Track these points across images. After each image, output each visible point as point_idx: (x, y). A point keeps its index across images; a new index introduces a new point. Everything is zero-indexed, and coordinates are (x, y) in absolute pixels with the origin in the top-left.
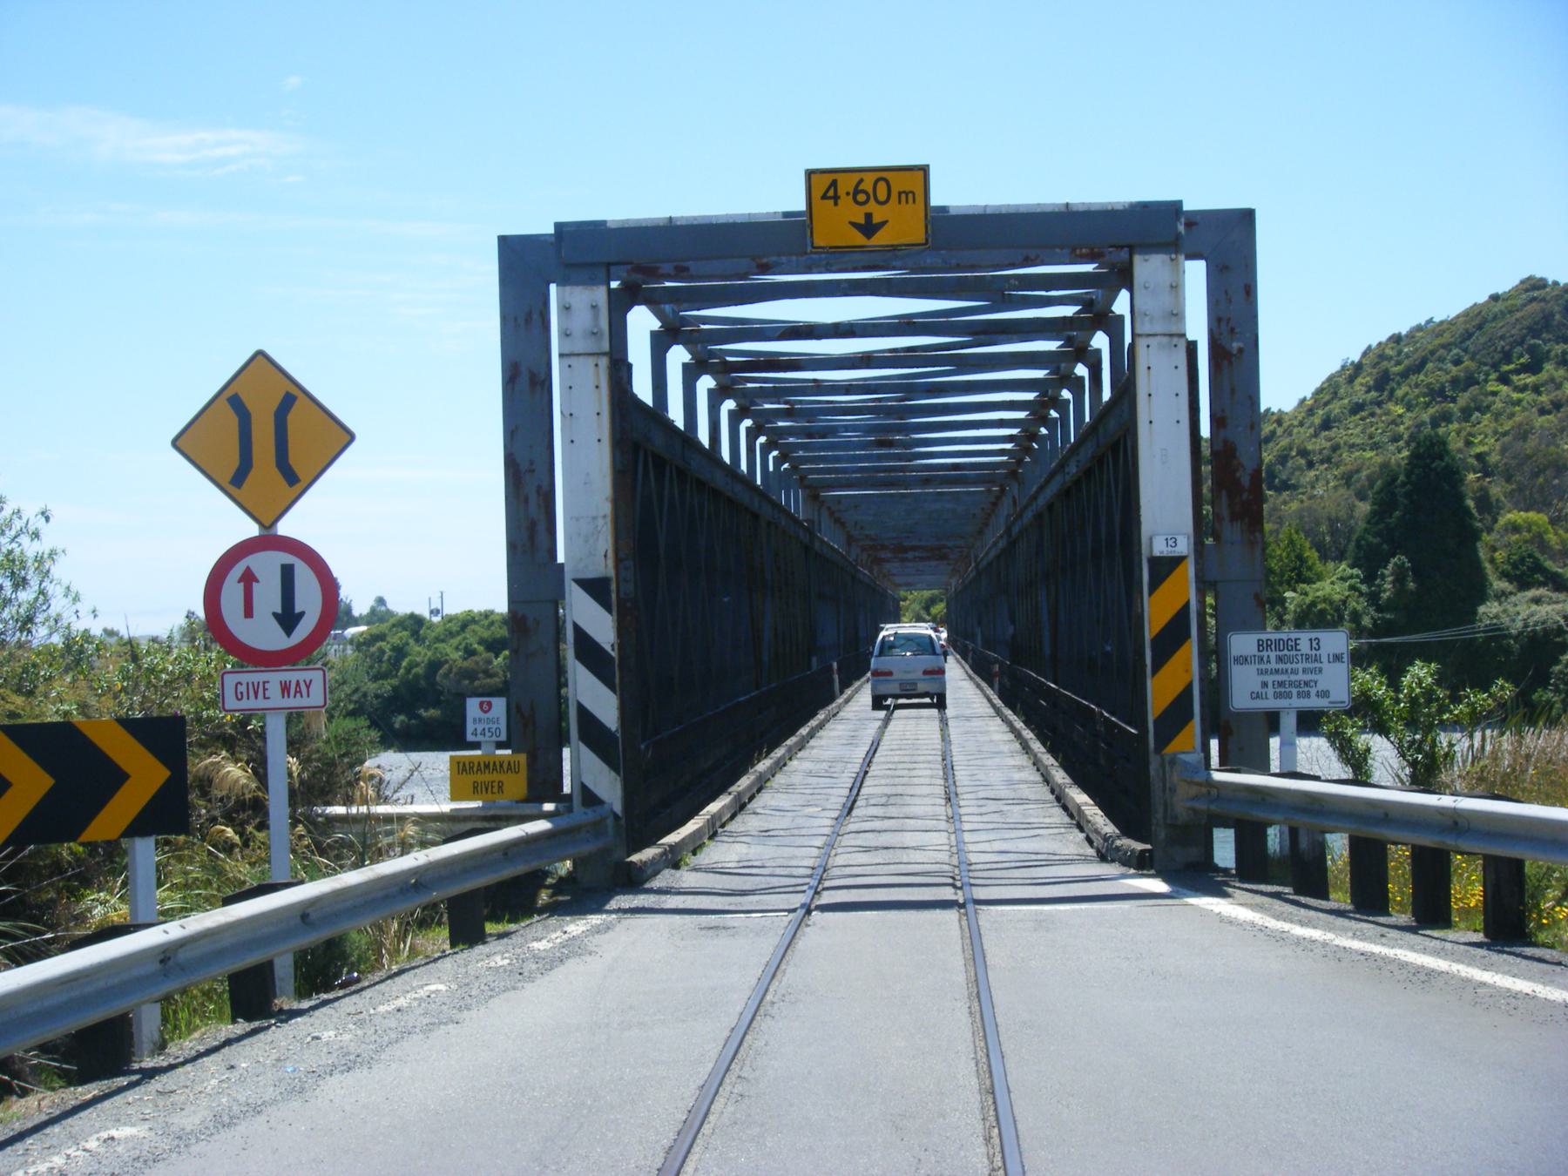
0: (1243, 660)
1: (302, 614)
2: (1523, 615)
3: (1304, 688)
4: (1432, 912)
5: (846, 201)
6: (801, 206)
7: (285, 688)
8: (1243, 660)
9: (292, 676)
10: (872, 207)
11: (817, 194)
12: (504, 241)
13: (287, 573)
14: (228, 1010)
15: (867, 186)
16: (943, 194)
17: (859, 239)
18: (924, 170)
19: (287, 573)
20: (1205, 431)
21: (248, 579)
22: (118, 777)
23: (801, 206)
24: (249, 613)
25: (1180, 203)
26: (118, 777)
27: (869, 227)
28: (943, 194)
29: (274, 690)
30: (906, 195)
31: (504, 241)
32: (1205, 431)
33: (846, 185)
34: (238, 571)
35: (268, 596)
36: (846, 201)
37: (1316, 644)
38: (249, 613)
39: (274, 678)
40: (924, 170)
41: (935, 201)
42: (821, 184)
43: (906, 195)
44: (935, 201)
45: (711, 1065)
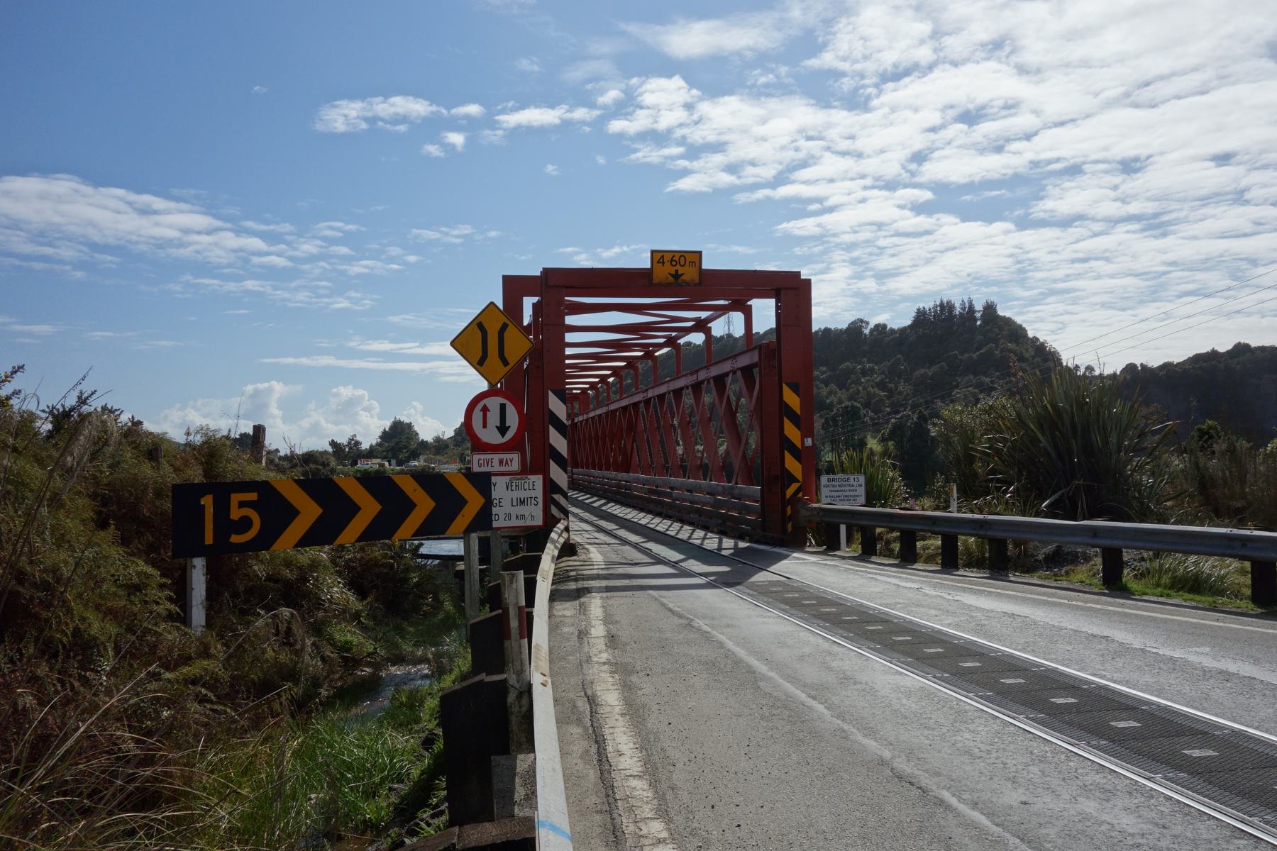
1: (333, 443)
4: (908, 557)
6: (649, 266)
7: (501, 462)
9: (504, 456)
10: (678, 267)
11: (656, 260)
12: (505, 278)
13: (503, 407)
14: (1098, 580)
15: (676, 258)
18: (700, 253)
21: (485, 410)
22: (354, 509)
23: (649, 266)
24: (485, 426)
25: (798, 273)
26: (354, 509)
27: (676, 276)
28: (706, 265)
29: (496, 463)
31: (505, 278)
34: (480, 406)
35: (494, 419)
38: (485, 426)
39: (496, 457)
40: (700, 253)
41: (704, 266)
44: (704, 266)
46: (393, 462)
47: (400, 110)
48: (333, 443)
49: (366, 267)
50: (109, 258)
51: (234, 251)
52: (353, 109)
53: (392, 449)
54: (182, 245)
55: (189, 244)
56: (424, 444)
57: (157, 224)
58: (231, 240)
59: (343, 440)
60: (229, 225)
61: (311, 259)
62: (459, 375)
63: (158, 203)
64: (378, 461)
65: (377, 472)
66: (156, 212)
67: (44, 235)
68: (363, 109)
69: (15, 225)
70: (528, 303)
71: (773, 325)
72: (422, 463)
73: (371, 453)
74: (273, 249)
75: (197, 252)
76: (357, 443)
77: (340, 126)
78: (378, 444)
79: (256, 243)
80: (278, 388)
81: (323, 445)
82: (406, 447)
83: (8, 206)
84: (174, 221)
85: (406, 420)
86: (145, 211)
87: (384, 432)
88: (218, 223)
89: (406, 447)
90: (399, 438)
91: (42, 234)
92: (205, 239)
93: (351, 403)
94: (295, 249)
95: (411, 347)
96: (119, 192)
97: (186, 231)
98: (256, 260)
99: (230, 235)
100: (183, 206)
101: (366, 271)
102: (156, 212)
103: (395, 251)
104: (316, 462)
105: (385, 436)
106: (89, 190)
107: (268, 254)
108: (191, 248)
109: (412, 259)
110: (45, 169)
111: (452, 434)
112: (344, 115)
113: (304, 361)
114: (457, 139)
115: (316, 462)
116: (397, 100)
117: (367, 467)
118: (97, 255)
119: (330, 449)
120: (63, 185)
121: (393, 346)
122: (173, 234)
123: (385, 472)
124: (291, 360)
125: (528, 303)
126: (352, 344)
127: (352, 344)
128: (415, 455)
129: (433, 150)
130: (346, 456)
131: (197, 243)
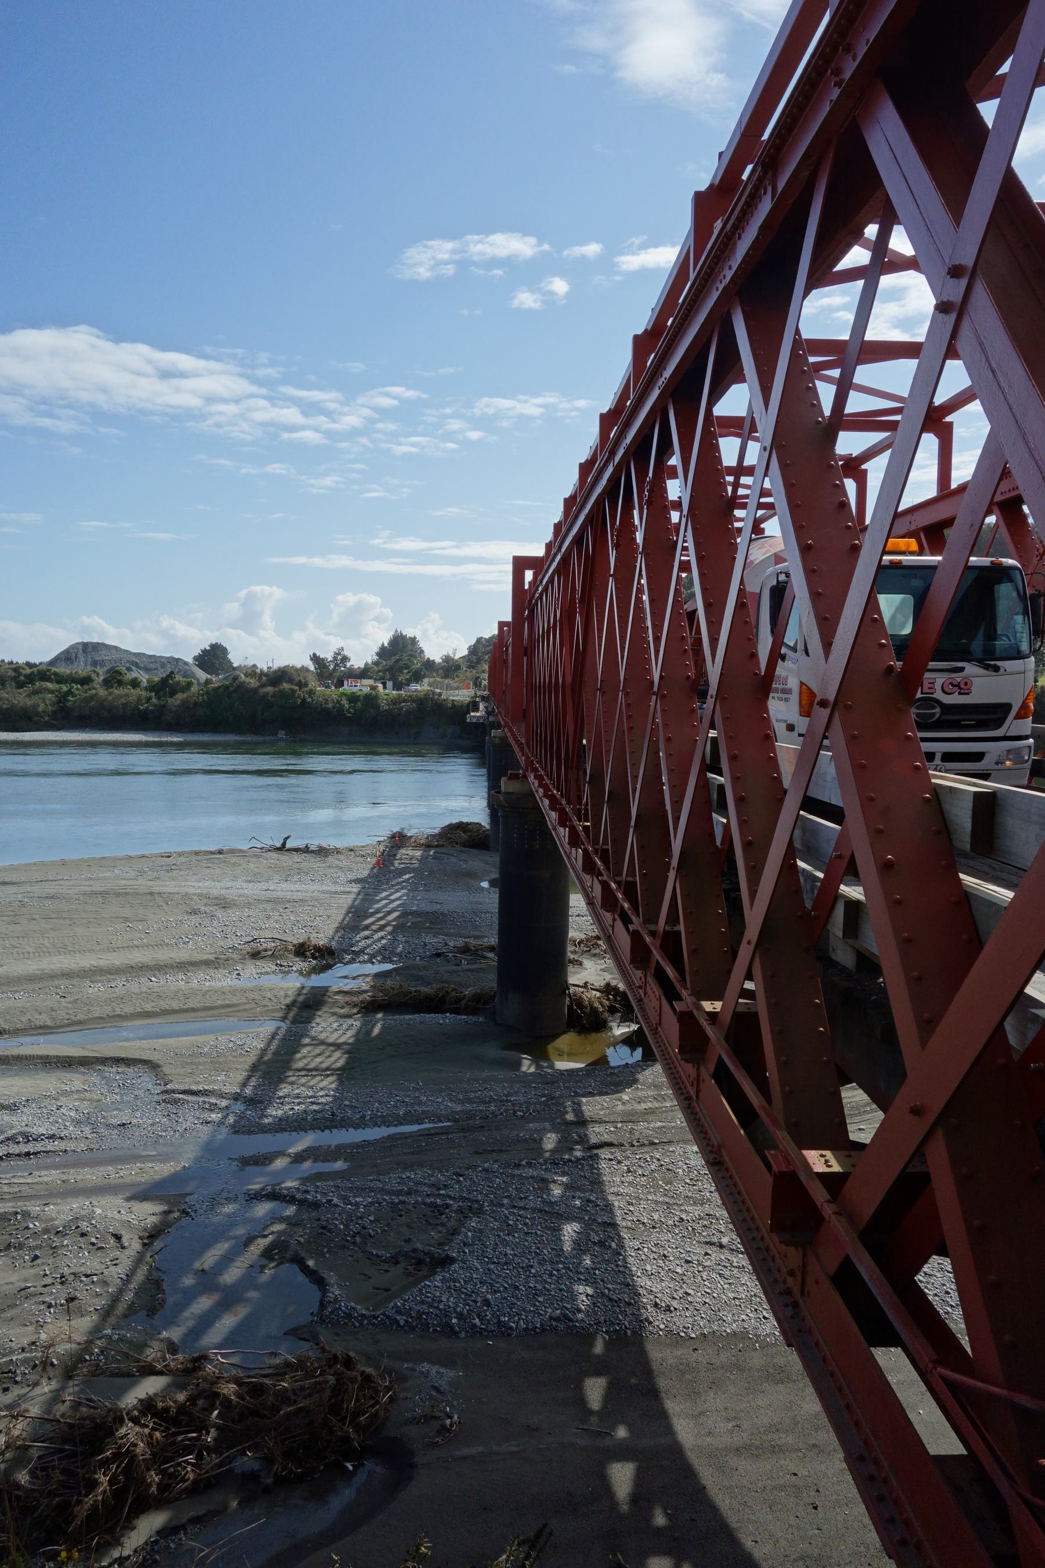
1: (315, 658)
46: (390, 684)
47: (502, 253)
48: (315, 658)
49: (413, 445)
50: (115, 431)
51: (263, 424)
52: (444, 249)
53: (390, 669)
54: (202, 416)
55: (211, 414)
56: (429, 664)
57: (178, 390)
58: (265, 412)
59: (328, 655)
60: (264, 391)
61: (353, 433)
62: (495, 582)
63: (183, 361)
64: (370, 682)
65: (367, 697)
66: (183, 375)
67: (47, 404)
68: (454, 252)
69: (15, 390)
70: (529, 575)
71: (496, 632)
72: (426, 687)
73: (364, 673)
74: (310, 421)
75: (218, 425)
76: (345, 659)
77: (424, 272)
78: (376, 663)
79: (291, 415)
80: (277, 593)
81: (301, 659)
82: (407, 667)
83: (18, 370)
84: (204, 384)
85: (409, 633)
86: (166, 374)
87: (383, 648)
88: (253, 389)
89: (407, 667)
90: (366, 664)
91: (44, 401)
92: (231, 409)
93: (359, 608)
94: (334, 421)
95: (446, 547)
96: (144, 349)
97: (211, 399)
98: (286, 436)
99: (263, 403)
100: (213, 365)
101: (413, 450)
102: (183, 375)
103: (455, 425)
104: (291, 681)
105: (383, 653)
106: (108, 346)
107: (303, 428)
108: (209, 422)
109: (474, 435)
110: (63, 321)
111: (465, 652)
112: (427, 258)
113: (317, 561)
114: (560, 286)
115: (291, 681)
116: (498, 238)
117: (355, 689)
118: (102, 429)
119: (312, 667)
120: (79, 339)
121: (425, 545)
122: (194, 402)
123: (377, 697)
124: (301, 560)
125: (529, 575)
126: (377, 541)
127: (377, 541)
128: (417, 677)
129: (526, 299)
130: (330, 676)
131: (221, 413)
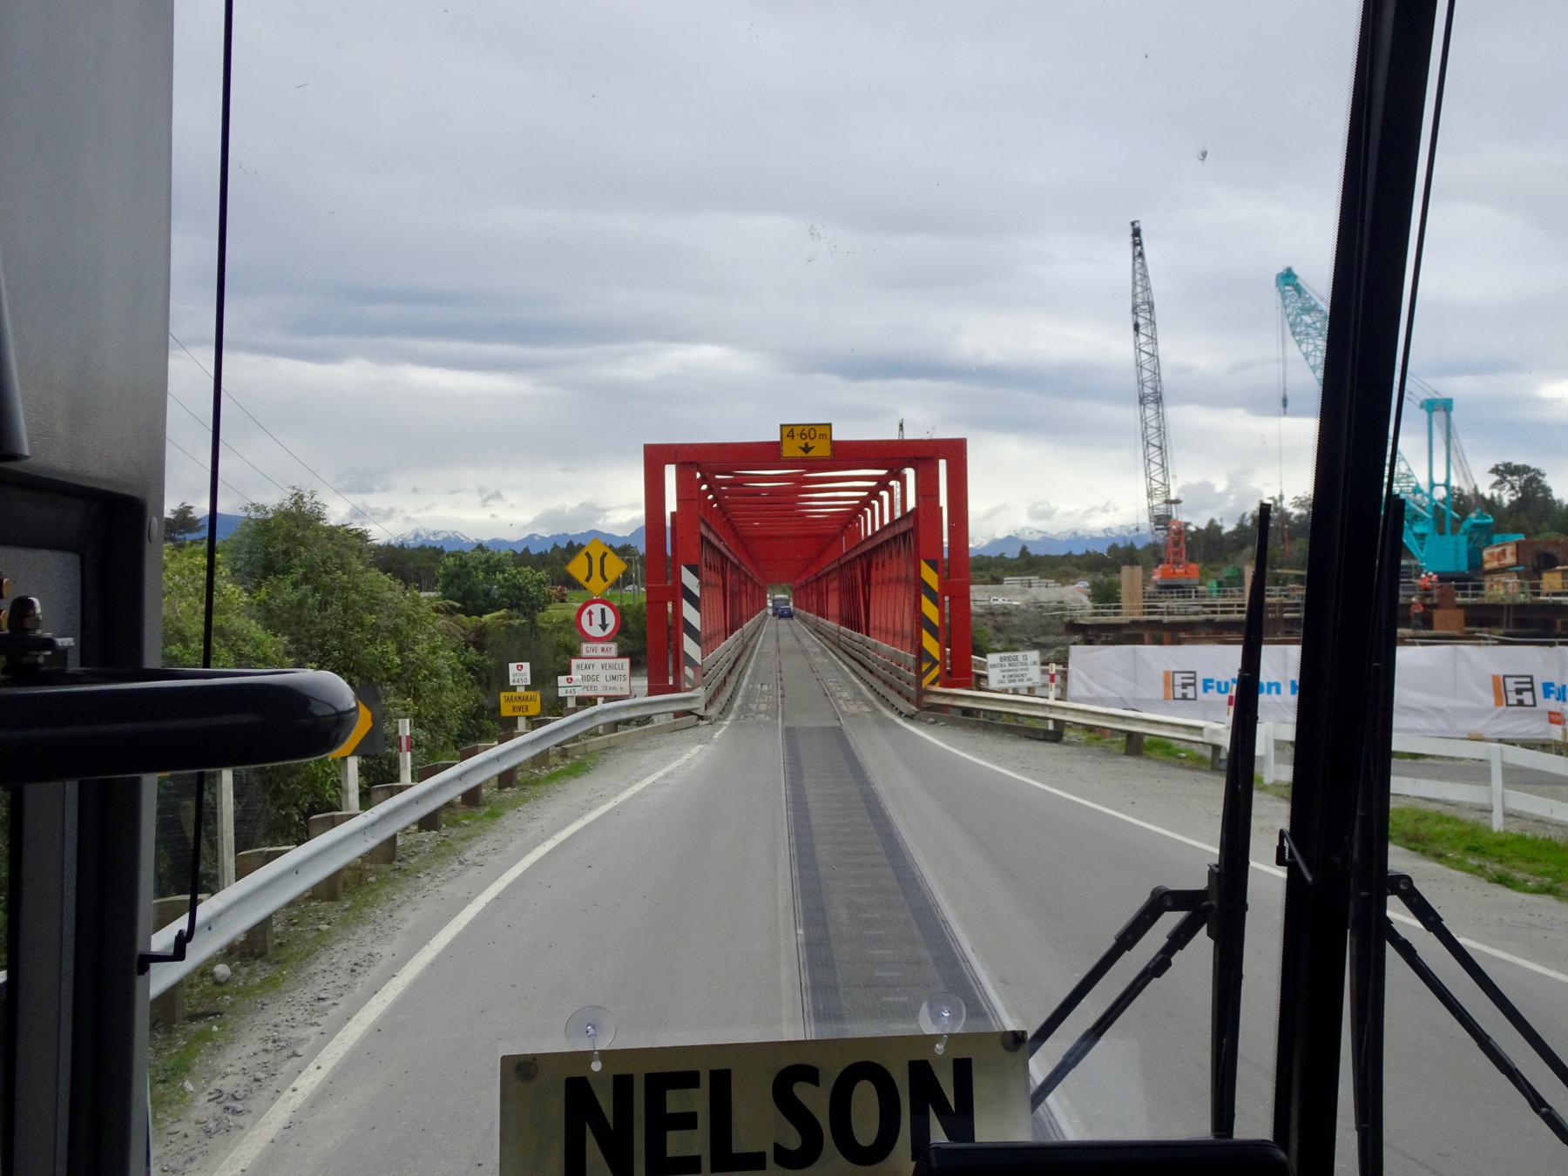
0: (994, 666)
2: (443, 621)
3: (1021, 678)
5: (797, 437)
8: (994, 666)
13: (603, 611)
16: (837, 436)
17: (802, 454)
19: (603, 611)
20: (671, 505)
21: (590, 613)
27: (806, 449)
30: (823, 436)
32: (671, 505)
33: (797, 431)
36: (797, 437)
37: (1025, 658)
42: (787, 431)
43: (823, 436)
44: (835, 438)
45: (1259, 751)
